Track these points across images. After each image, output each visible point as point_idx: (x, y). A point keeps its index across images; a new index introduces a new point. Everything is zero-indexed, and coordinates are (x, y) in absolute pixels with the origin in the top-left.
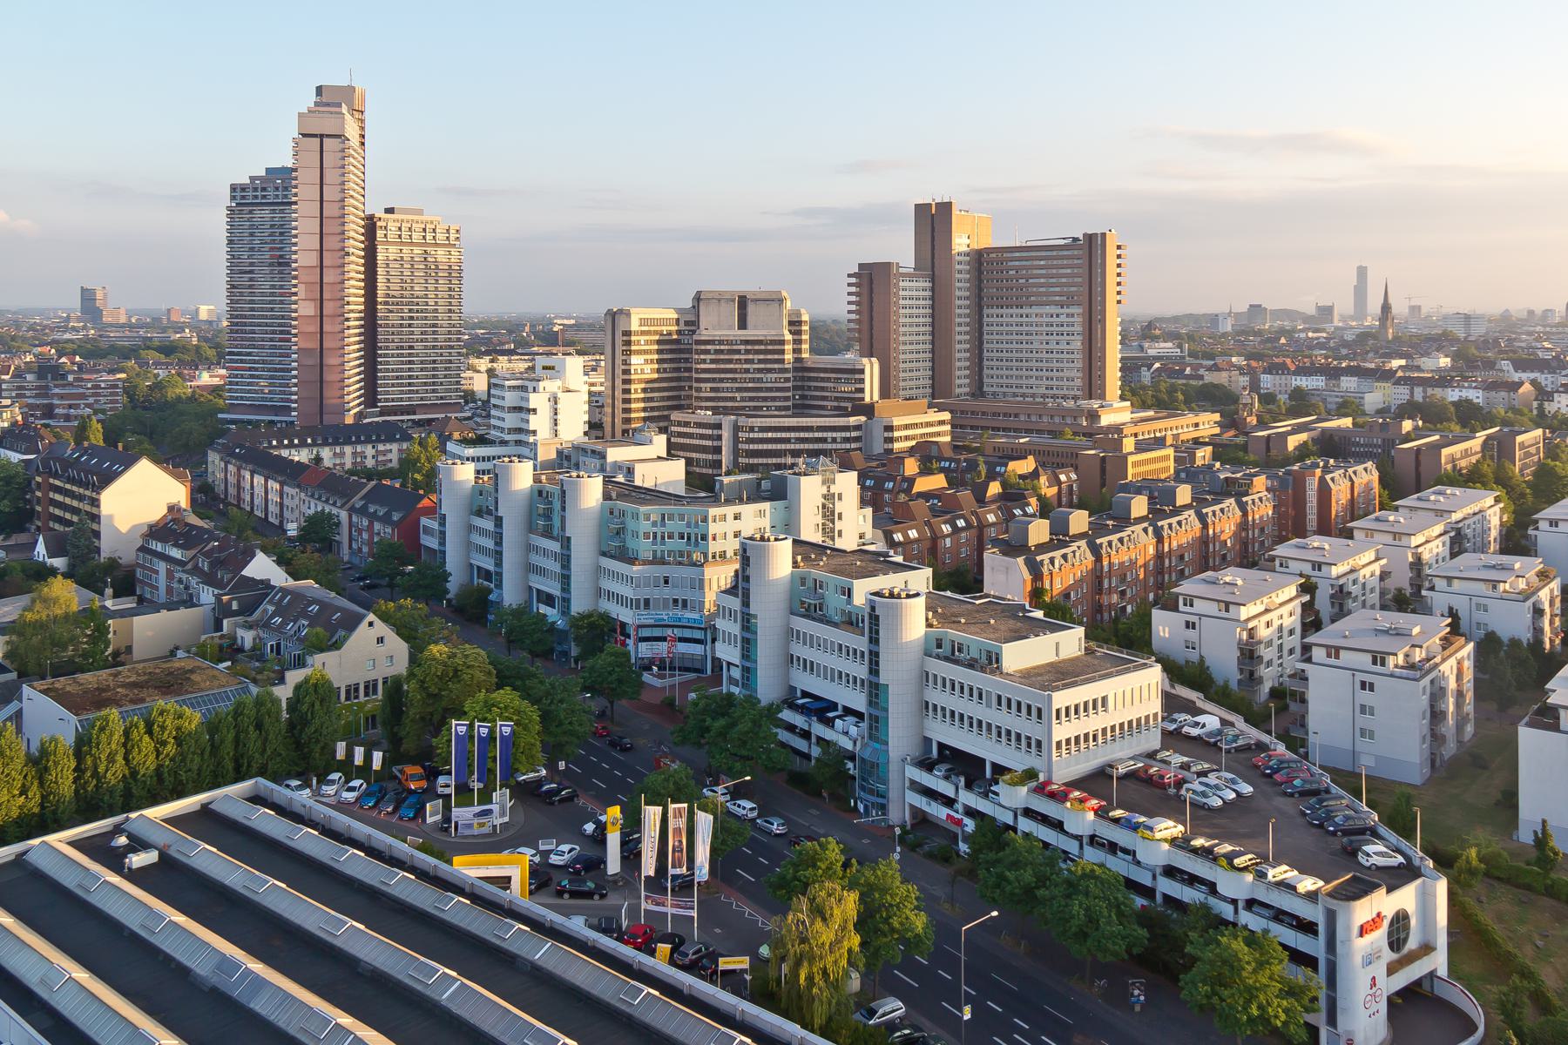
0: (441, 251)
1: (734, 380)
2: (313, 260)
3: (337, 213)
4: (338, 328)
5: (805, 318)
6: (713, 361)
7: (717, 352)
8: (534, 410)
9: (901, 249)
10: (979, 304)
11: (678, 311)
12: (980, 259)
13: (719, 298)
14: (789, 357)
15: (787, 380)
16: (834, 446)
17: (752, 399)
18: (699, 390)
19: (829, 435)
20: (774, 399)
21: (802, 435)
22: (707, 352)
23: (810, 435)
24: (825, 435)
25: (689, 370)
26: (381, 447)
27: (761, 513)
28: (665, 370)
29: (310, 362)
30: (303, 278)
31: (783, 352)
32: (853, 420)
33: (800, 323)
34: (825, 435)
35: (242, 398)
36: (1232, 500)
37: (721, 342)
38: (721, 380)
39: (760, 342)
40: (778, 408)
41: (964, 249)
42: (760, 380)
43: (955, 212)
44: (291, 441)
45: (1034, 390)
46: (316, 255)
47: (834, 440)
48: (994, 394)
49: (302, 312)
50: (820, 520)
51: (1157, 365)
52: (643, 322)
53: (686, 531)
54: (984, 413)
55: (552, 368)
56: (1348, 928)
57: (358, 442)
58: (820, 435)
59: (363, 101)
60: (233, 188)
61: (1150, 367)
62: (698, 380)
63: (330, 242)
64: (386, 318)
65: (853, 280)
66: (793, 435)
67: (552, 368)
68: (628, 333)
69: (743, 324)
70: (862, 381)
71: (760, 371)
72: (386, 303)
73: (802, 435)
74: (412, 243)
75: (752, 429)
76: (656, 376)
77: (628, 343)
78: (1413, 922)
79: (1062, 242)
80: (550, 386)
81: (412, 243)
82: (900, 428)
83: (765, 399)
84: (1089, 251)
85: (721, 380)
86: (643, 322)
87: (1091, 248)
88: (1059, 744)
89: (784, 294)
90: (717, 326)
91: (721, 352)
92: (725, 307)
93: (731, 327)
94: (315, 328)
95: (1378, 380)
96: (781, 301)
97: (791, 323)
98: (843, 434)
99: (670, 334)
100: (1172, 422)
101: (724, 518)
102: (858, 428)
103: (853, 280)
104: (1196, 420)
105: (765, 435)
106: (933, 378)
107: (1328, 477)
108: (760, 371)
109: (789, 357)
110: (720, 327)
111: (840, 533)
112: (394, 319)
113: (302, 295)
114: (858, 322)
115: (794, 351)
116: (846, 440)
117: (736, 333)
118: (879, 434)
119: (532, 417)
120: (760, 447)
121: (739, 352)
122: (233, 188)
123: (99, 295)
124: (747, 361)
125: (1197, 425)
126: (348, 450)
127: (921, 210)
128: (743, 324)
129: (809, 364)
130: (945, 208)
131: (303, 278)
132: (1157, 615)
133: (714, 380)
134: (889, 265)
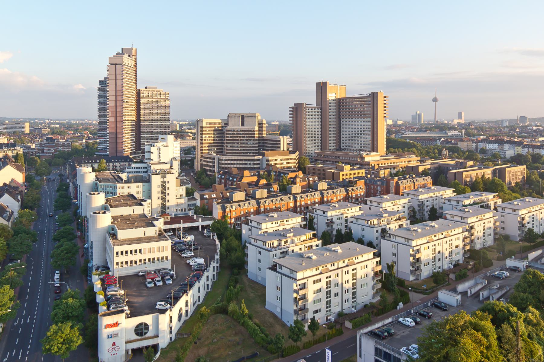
0: (162, 100)
1: (238, 143)
2: (113, 104)
3: (120, 89)
4: (121, 125)
5: (264, 122)
6: (231, 137)
7: (233, 134)
8: (152, 153)
9: (311, 100)
10: (339, 117)
11: (221, 120)
12: (340, 102)
13: (235, 116)
14: (257, 136)
15: (257, 143)
16: (250, 166)
17: (244, 150)
18: (227, 146)
19: (248, 162)
20: (251, 150)
21: (239, 162)
22: (229, 134)
23: (242, 162)
24: (247, 162)
25: (224, 140)
26: (122, 164)
27: (138, 187)
28: (216, 140)
30: (110, 110)
31: (254, 134)
32: (256, 158)
33: (262, 124)
34: (247, 162)
36: (344, 188)
38: (234, 143)
39: (249, 131)
40: (253, 153)
41: (334, 98)
42: (247, 143)
44: (92, 161)
45: (356, 148)
47: (250, 164)
48: (344, 149)
49: (110, 120)
50: (160, 189)
51: (443, 139)
52: (207, 124)
53: (112, 191)
55: (164, 139)
56: (101, 325)
57: (115, 162)
58: (245, 162)
60: (100, 81)
61: (440, 140)
62: (227, 143)
63: (119, 98)
64: (144, 122)
65: (291, 109)
66: (236, 162)
67: (164, 139)
68: (202, 127)
69: (243, 125)
70: (280, 144)
71: (247, 140)
72: (144, 118)
73: (239, 162)
74: (161, 98)
76: (213, 142)
77: (202, 131)
78: (151, 328)
79: (365, 95)
80: (160, 144)
81: (152, 98)
82: (272, 160)
83: (249, 150)
84: (373, 96)
85: (234, 143)
86: (207, 124)
87: (373, 96)
88: (117, 264)
89: (257, 114)
90: (235, 125)
92: (237, 119)
93: (239, 126)
94: (114, 125)
95: (517, 146)
96: (255, 117)
97: (259, 124)
98: (253, 162)
99: (218, 127)
100: (400, 160)
101: (123, 188)
102: (259, 160)
103: (291, 109)
105: (227, 162)
106: (322, 143)
107: (400, 182)
108: (247, 140)
109: (257, 136)
111: (168, 194)
112: (147, 123)
113: (110, 115)
114: (293, 124)
115: (259, 134)
116: (254, 164)
117: (241, 128)
118: (265, 163)
119: (152, 154)
120: (225, 166)
121: (240, 134)
122: (100, 81)
124: (243, 137)
125: (410, 161)
126: (111, 164)
127: (318, 84)
128: (243, 125)
129: (265, 138)
130: (325, 84)
132: (243, 226)
133: (232, 143)
134: (302, 104)
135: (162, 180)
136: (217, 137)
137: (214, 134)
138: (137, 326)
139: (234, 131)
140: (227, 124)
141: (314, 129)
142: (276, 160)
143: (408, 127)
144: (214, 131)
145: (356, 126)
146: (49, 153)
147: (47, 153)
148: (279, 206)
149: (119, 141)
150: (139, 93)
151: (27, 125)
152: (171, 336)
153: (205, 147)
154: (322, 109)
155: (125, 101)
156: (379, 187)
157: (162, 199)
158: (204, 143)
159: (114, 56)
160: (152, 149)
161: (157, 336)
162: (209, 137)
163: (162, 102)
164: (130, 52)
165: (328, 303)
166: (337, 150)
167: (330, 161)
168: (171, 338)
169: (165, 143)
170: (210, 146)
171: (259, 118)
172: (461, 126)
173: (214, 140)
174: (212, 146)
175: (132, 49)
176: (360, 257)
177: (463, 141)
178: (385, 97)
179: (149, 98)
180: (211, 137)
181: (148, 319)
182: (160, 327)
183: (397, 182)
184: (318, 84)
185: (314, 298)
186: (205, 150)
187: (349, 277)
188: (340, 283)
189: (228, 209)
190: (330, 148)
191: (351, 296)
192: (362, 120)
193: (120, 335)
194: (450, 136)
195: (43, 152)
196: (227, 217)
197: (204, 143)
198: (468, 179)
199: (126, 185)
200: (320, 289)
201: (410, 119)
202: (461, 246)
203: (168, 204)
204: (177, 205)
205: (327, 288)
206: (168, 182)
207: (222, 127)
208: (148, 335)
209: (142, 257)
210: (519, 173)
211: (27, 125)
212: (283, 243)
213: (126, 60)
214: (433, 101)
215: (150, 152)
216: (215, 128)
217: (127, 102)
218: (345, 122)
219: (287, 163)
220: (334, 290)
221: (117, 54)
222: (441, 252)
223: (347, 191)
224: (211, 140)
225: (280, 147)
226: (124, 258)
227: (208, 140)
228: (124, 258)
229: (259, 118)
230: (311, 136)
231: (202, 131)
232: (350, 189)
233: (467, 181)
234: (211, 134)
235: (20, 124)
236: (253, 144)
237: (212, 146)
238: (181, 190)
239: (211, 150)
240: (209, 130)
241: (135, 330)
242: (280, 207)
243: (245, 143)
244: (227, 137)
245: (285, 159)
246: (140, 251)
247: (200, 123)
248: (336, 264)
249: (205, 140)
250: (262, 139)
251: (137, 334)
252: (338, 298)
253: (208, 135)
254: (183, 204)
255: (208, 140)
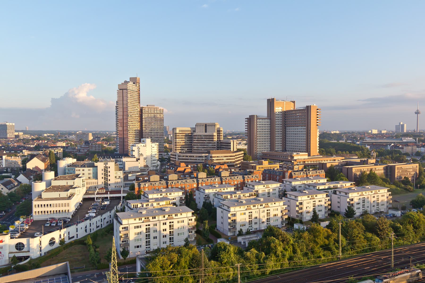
0: (158, 115)
3: (126, 107)
6: (197, 140)
7: (198, 138)
9: (263, 112)
11: (191, 128)
12: (285, 114)
22: (195, 138)
27: (89, 170)
28: (187, 143)
29: (121, 140)
33: (220, 131)
35: (239, 157)
37: (199, 136)
42: (208, 145)
43: (275, 101)
46: (122, 116)
47: (199, 160)
51: (393, 144)
52: (180, 131)
54: (275, 156)
57: (117, 158)
59: (139, 81)
62: (194, 145)
63: (125, 113)
65: (247, 120)
68: (176, 134)
69: (206, 132)
70: (230, 146)
75: (183, 156)
77: (176, 136)
78: (26, 246)
81: (151, 113)
82: (215, 157)
86: (180, 131)
87: (308, 108)
89: (216, 124)
90: (200, 132)
91: (199, 138)
93: (203, 132)
94: (122, 133)
96: (214, 125)
97: (218, 131)
101: (79, 170)
102: (206, 157)
103: (247, 120)
104: (334, 159)
106: (270, 146)
108: (208, 143)
110: (200, 132)
111: (109, 176)
112: (147, 131)
115: (217, 138)
121: (203, 138)
123: (167, 128)
127: (268, 100)
130: (273, 99)
131: (120, 122)
133: (197, 145)
135: (105, 166)
136: (187, 140)
137: (185, 138)
138: (17, 244)
139: (201, 136)
140: (195, 131)
141: (264, 135)
142: (218, 157)
143: (389, 136)
144: (185, 136)
145: (295, 132)
146: (83, 152)
147: (81, 152)
148: (183, 186)
149: (125, 144)
150: (141, 110)
151: (90, 134)
152: (41, 253)
153: (178, 147)
154: (270, 119)
155: (129, 115)
156: (278, 177)
157: (105, 178)
158: (178, 145)
159: (122, 84)
160: (134, 148)
161: (29, 252)
162: (181, 140)
163: (158, 116)
164: (134, 81)
165: (148, 243)
166: (283, 151)
167: (277, 160)
168: (41, 254)
169: (144, 144)
170: (182, 147)
171: (218, 126)
172: (413, 135)
173: (185, 143)
174: (183, 147)
175: (136, 78)
176: (179, 215)
177: (408, 146)
178: (318, 109)
179: (149, 113)
180: (183, 140)
181: (24, 241)
182: (30, 246)
183: (291, 174)
184: (268, 100)
185: (135, 238)
186: (178, 150)
187: (167, 227)
188: (158, 230)
189: (142, 186)
190: (276, 150)
191: (168, 240)
192: (300, 127)
193: (4, 248)
194: (405, 142)
195: (80, 152)
196: (142, 191)
197: (178, 145)
198: (358, 173)
199: (81, 169)
200: (141, 232)
201: (394, 129)
202: (280, 215)
203: (109, 182)
204: (115, 183)
205: (146, 232)
206: (109, 167)
207: (191, 133)
208: (23, 250)
209: (52, 209)
210: (412, 170)
211: (90, 134)
212: (145, 206)
213: (131, 86)
214: (416, 113)
215: (133, 151)
216: (186, 134)
217: (131, 116)
218: (290, 130)
219: (227, 159)
220: (152, 235)
221: (125, 82)
222: (258, 218)
223: (244, 178)
224: (183, 143)
225: (230, 148)
226: (40, 209)
227: (180, 143)
228: (40, 209)
229: (218, 126)
230: (261, 140)
231: (176, 136)
232: (246, 176)
233: (357, 175)
234: (183, 138)
235: (85, 134)
236: (212, 145)
237: (183, 147)
238: (119, 173)
239: (183, 150)
240: (181, 136)
241: (16, 247)
242: (185, 187)
243: (206, 145)
244: (194, 140)
245: (225, 157)
246: (50, 205)
247: (174, 130)
248: (157, 217)
249: (178, 143)
250: (219, 141)
251: (17, 249)
252: (157, 241)
253: (180, 139)
254: (119, 183)
255: (180, 143)
